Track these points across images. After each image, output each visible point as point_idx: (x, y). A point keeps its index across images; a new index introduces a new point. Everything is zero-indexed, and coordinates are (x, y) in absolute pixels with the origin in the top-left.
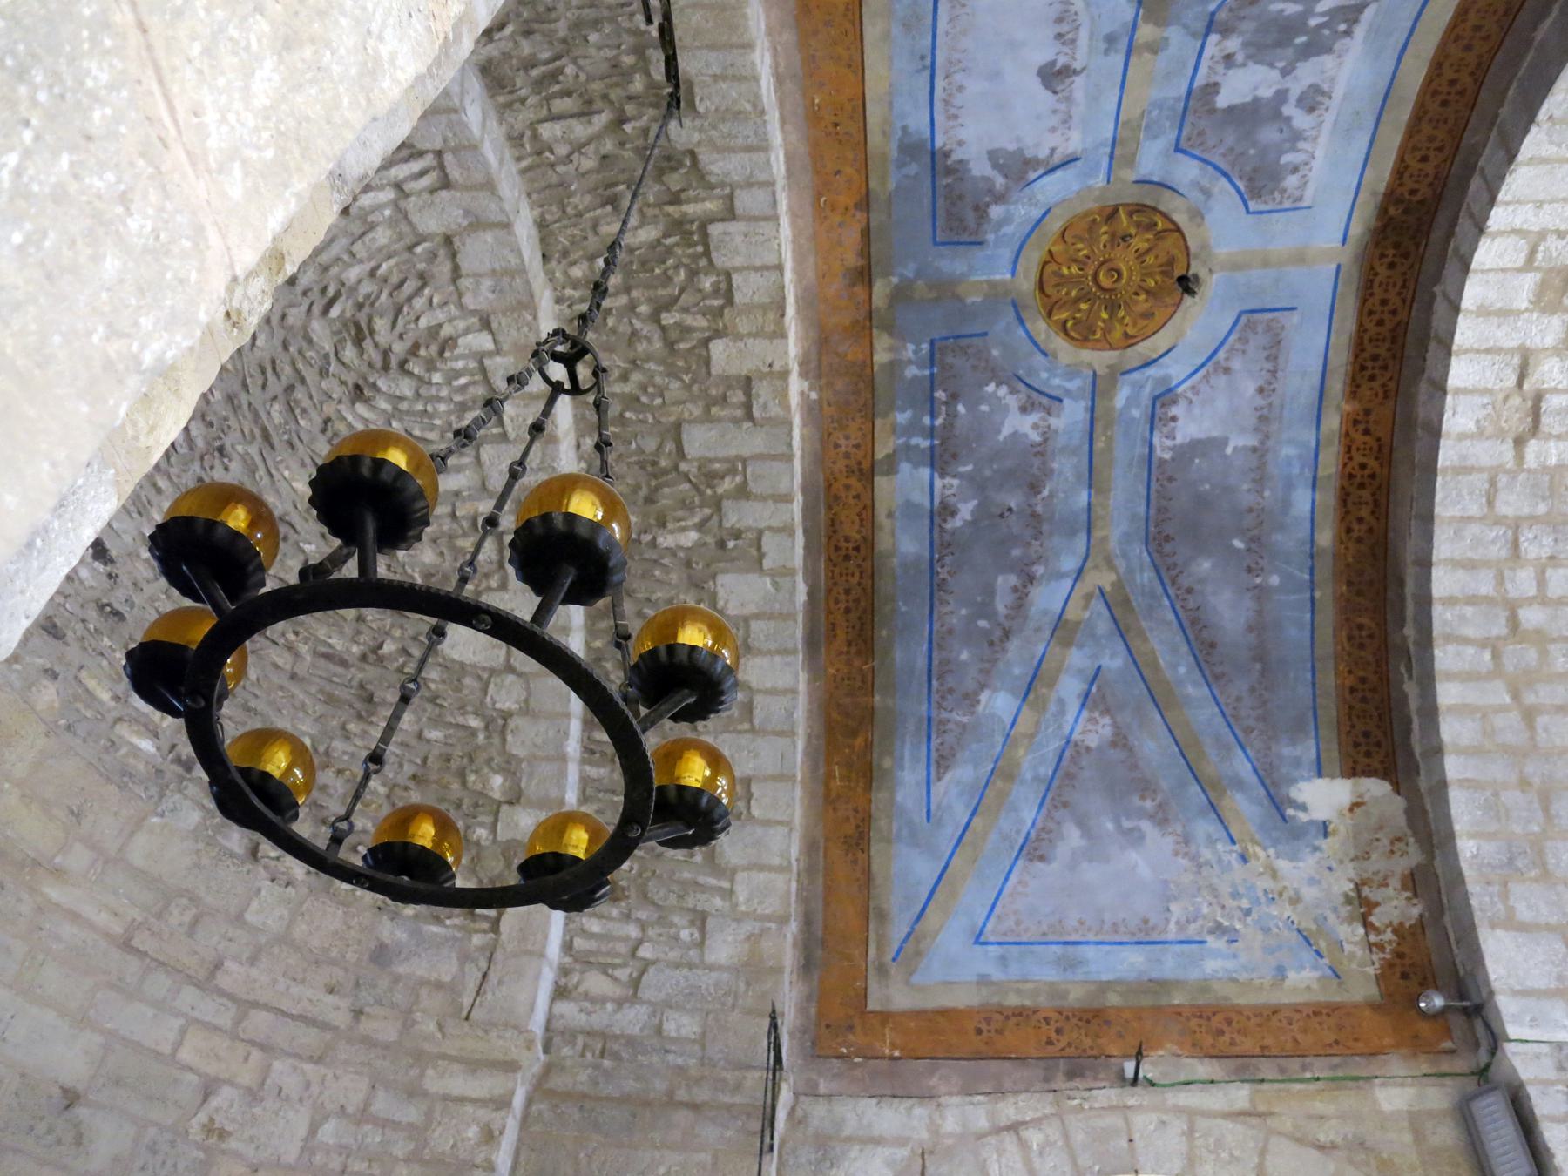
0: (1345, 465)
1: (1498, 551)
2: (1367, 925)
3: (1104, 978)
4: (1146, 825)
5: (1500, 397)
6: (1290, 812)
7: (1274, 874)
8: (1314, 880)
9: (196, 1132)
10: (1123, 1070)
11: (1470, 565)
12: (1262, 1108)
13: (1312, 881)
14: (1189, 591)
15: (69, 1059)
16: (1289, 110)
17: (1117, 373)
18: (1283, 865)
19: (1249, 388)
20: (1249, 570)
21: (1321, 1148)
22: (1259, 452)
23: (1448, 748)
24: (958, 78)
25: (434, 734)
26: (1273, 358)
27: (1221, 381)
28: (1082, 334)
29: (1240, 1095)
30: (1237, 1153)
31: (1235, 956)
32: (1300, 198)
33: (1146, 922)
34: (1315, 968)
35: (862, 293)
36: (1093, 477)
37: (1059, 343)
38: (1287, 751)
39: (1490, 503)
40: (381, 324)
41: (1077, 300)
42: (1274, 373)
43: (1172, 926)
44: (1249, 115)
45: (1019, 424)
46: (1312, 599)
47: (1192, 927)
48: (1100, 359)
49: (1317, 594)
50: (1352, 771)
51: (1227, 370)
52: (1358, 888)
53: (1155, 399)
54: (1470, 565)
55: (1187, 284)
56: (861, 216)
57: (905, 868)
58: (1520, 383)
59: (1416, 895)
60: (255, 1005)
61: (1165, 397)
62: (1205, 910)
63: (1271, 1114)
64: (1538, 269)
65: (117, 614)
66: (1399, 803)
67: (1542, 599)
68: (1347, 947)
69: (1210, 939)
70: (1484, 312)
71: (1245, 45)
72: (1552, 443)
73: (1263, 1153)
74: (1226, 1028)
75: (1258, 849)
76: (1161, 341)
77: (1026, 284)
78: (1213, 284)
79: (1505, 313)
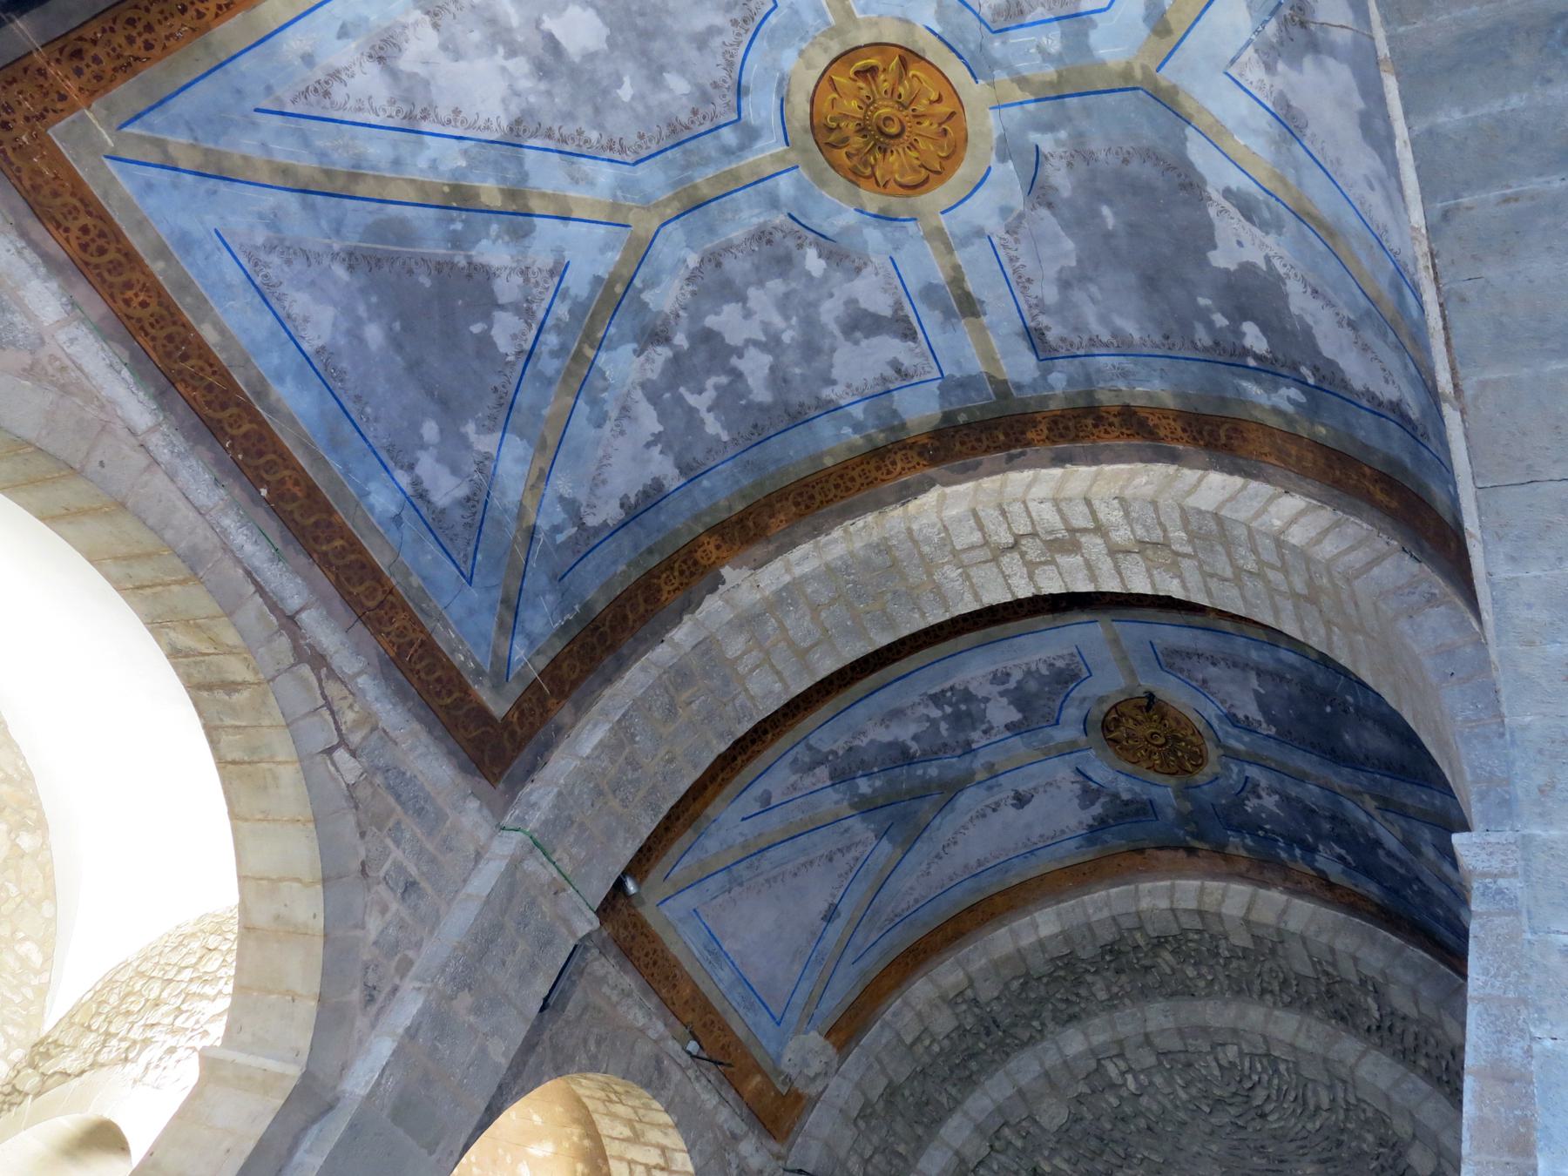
16: (1012, 684)
17: (1219, 744)
22: (1260, 673)
24: (1034, 840)
26: (1189, 655)
28: (1199, 759)
32: (1072, 655)
40: (1217, 1092)
42: (1199, 656)
44: (1020, 699)
48: (1213, 753)
51: (1204, 682)
55: (1151, 696)
56: (1148, 852)
61: (1232, 719)
70: (1093, 578)
71: (974, 729)
76: (1193, 716)
77: (1172, 781)
78: (1146, 684)
79: (1089, 566)
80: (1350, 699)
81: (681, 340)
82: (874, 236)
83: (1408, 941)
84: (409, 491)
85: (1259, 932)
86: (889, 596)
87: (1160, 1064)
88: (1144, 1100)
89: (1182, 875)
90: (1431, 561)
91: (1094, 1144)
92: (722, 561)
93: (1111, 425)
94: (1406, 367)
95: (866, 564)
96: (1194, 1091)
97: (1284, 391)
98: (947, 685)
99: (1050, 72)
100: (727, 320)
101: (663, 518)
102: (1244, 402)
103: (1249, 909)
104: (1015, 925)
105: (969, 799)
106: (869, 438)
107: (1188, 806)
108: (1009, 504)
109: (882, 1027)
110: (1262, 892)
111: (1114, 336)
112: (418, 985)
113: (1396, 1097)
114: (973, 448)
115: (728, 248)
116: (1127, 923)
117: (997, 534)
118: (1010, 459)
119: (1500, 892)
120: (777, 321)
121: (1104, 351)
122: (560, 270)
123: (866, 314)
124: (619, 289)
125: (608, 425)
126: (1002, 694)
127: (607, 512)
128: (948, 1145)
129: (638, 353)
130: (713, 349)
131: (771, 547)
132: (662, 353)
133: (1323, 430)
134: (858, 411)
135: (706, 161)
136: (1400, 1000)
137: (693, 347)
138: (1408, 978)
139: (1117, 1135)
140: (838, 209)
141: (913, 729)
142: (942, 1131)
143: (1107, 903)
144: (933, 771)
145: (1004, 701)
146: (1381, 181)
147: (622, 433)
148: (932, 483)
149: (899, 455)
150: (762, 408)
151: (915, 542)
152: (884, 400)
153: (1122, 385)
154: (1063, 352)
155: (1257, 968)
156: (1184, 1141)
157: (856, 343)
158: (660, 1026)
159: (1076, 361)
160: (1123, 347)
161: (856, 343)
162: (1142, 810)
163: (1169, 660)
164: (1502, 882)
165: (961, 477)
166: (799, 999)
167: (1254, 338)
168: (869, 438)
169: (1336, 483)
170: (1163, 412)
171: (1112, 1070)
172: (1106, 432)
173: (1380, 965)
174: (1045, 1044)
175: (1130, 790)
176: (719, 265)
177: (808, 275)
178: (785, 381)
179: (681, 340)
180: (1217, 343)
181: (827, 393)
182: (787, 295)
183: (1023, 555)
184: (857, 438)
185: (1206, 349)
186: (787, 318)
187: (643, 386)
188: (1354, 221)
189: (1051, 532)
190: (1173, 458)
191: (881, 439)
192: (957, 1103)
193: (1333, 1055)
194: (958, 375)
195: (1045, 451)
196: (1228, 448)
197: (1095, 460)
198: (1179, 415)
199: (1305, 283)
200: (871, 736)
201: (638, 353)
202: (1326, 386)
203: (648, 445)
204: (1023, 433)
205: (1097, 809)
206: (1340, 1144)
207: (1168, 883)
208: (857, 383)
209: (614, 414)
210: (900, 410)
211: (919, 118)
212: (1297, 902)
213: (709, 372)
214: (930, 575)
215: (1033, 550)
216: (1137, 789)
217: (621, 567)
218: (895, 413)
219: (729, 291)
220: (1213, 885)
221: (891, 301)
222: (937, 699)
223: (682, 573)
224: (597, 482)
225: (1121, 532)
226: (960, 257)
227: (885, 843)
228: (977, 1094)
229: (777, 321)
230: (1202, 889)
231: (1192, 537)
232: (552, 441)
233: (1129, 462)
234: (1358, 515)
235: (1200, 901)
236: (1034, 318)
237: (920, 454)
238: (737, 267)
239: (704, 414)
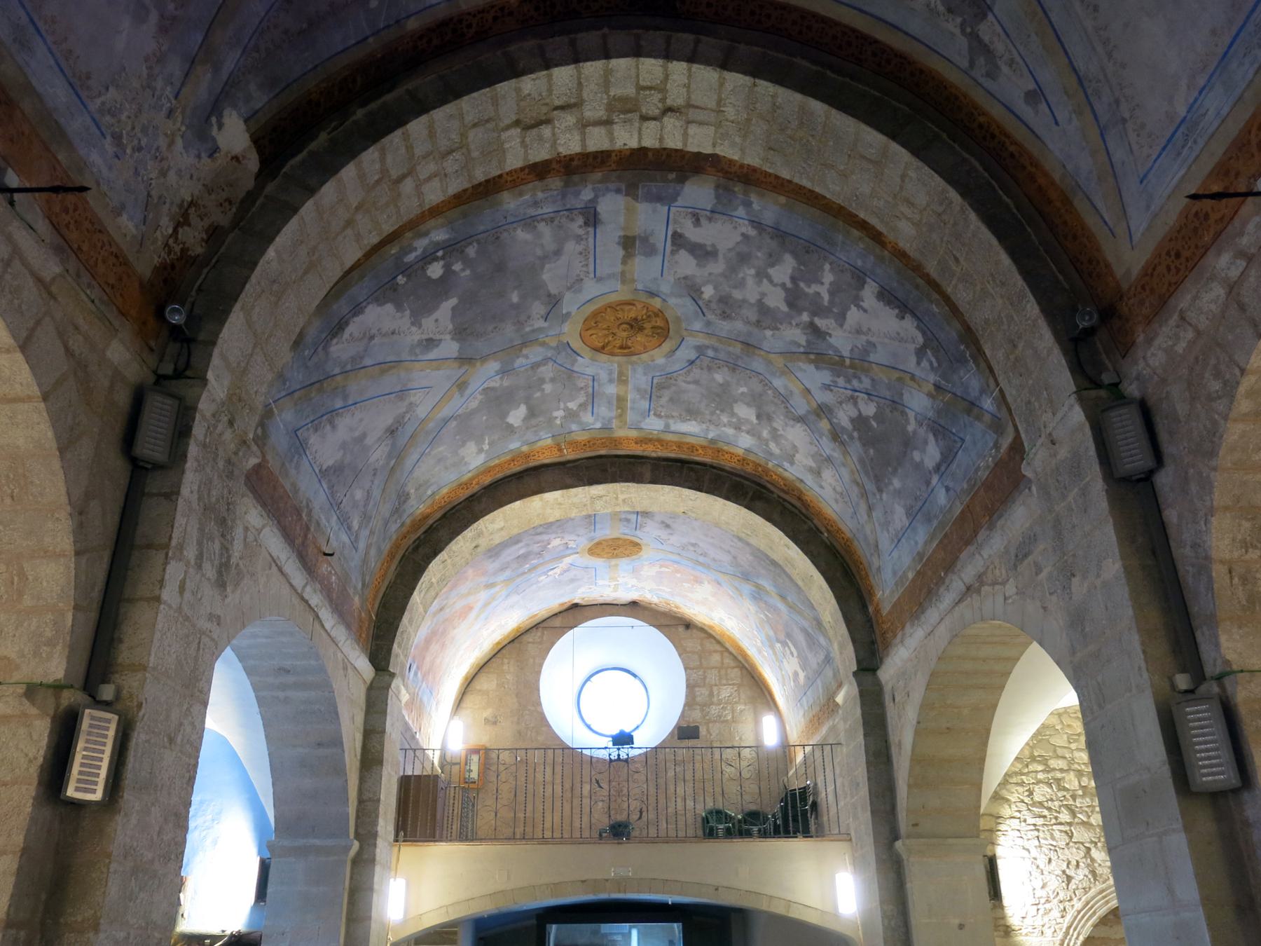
0: (469, 14)
1: (443, 144)
2: (175, 230)
3: (34, 82)
4: (154, 17)
5: (548, 101)
6: (214, 120)
7: (171, 144)
8: (182, 172)
10: (525, 419)
11: (432, 134)
12: (54, 289)
13: (179, 172)
18: (179, 143)
21: (67, 349)
23: (317, 196)
29: (51, 268)
30: (24, 307)
31: (110, 168)
33: (88, 78)
34: (137, 227)
38: (252, 87)
39: (475, 125)
43: (98, 101)
46: (367, 38)
47: (108, 118)
49: (371, 40)
50: (256, 141)
52: (191, 204)
54: (432, 134)
58: (556, 108)
59: (207, 242)
62: (123, 117)
63: (55, 299)
64: (638, 93)
66: (250, 184)
68: (158, 233)
69: (109, 138)
73: (38, 323)
74: (71, 211)
75: (180, 119)
81: (805, 317)
82: (665, 288)
86: (789, 132)
97: (419, 252)
99: (525, 351)
100: (776, 300)
115: (748, 322)
120: (750, 282)
122: (827, 387)
123: (695, 257)
124: (812, 357)
125: (873, 339)
129: (830, 335)
130: (794, 299)
132: (820, 323)
135: (729, 353)
137: (804, 309)
140: (679, 306)
149: (733, 170)
150: (795, 255)
153: (540, 195)
157: (713, 245)
158: (1225, 259)
159: (568, 206)
160: (530, 223)
161: (713, 245)
176: (758, 321)
177: (715, 288)
178: (770, 255)
179: (805, 317)
180: (463, 251)
181: (752, 232)
182: (735, 287)
183: (663, 100)
184: (754, 198)
186: (743, 279)
187: (841, 326)
191: (738, 188)
194: (658, 205)
201: (830, 335)
203: (865, 311)
209: (864, 338)
210: (713, 196)
211: (608, 328)
213: (806, 295)
214: (748, 120)
218: (717, 197)
219: (763, 309)
221: (677, 257)
226: (619, 268)
229: (750, 282)
236: (588, 233)
238: (753, 315)
239: (827, 286)
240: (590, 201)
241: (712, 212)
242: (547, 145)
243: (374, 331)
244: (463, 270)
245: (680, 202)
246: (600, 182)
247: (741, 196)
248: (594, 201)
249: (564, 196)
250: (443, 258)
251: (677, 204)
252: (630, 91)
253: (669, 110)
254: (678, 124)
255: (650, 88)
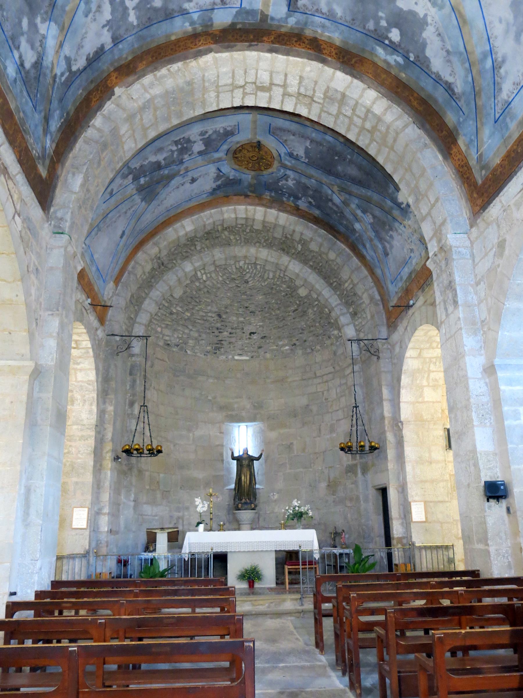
9: (324, 401)
14: (345, 175)
15: (304, 401)
19: (292, 137)
20: (344, 160)
22: (312, 141)
25: (315, 309)
26: (284, 131)
27: (289, 143)
35: (255, 193)
36: (310, 177)
37: (270, 170)
40: (233, 276)
41: (259, 164)
42: (289, 131)
45: (291, 183)
48: (276, 164)
51: (286, 140)
53: (290, 157)
57: (378, 272)
60: (323, 375)
61: (291, 155)
64: (256, 92)
65: (265, 337)
67: (365, 120)
72: (316, 94)
77: (253, 173)
78: (259, 138)
80: (349, 157)
83: (320, 227)
84: (19, 63)
85: (266, 225)
87: (216, 269)
88: (208, 283)
89: (240, 204)
90: (426, 131)
91: (189, 299)
92: (116, 84)
93: (304, 43)
94: (466, 76)
95: (182, 90)
96: (225, 277)
97: (395, 57)
98: (182, 136)
101: (100, 64)
102: (372, 52)
103: (265, 217)
104: (175, 226)
105: (174, 182)
106: (194, 29)
107: (255, 182)
108: (250, 70)
109: (129, 273)
110: (268, 210)
111: (329, 11)
112: (50, 313)
113: (301, 274)
114: (237, 39)
116: (218, 223)
117: (239, 81)
118: (250, 46)
119: (459, 252)
121: (321, 15)
125: (91, 15)
126: (201, 140)
127: (80, 64)
128: (146, 311)
131: (136, 77)
133: (404, 75)
134: (195, 16)
136: (313, 246)
138: (320, 240)
139: (197, 296)
141: (165, 155)
142: (143, 306)
143: (211, 216)
144: (166, 172)
145: (201, 142)
146: (508, 24)
147: (95, 20)
148: (210, 51)
149: (203, 38)
151: (204, 80)
152: (209, 13)
154: (301, 10)
155: (262, 236)
156: (218, 294)
159: (305, 16)
160: (331, 17)
162: (237, 182)
163: (272, 131)
164: (460, 249)
165: (224, 50)
166: (110, 271)
167: (395, 35)
168: (194, 29)
169: (396, 93)
170: (331, 45)
171: (199, 274)
172: (300, 45)
173: (311, 236)
174: (177, 268)
175: (235, 176)
180: (376, 30)
185: (369, 30)
188: (480, 24)
189: (261, 83)
190: (323, 61)
191: (199, 29)
192: (147, 294)
193: (280, 263)
194: (248, 8)
195: (267, 46)
196: (353, 66)
197: (287, 54)
198: (338, 48)
199: (437, 30)
200: (150, 159)
202: (418, 63)
203: (104, 26)
204: (262, 37)
205: (219, 183)
206: (272, 288)
207: (233, 207)
208: (201, 3)
212: (281, 214)
214: (204, 95)
215: (249, 89)
216: (237, 175)
217: (81, 91)
218: (211, 19)
220: (250, 208)
222: (176, 143)
223: (101, 91)
224: (80, 47)
225: (293, 89)
227: (143, 203)
228: (153, 290)
230: (246, 210)
231: (326, 96)
232: (66, 25)
233: (302, 58)
234: (399, 105)
235: (247, 214)
237: (212, 39)
239: (131, 9)
240: (291, 16)
241: (213, 9)
242: (304, 84)
243: (445, 54)
244: (381, 18)
245: (234, 11)
246: (283, 26)
247: (197, 26)
248: (288, 16)
249: (306, 24)
250: (387, 38)
251: (237, 9)
252: (259, 93)
253: (242, 87)
254: (237, 82)
255: (251, 94)
